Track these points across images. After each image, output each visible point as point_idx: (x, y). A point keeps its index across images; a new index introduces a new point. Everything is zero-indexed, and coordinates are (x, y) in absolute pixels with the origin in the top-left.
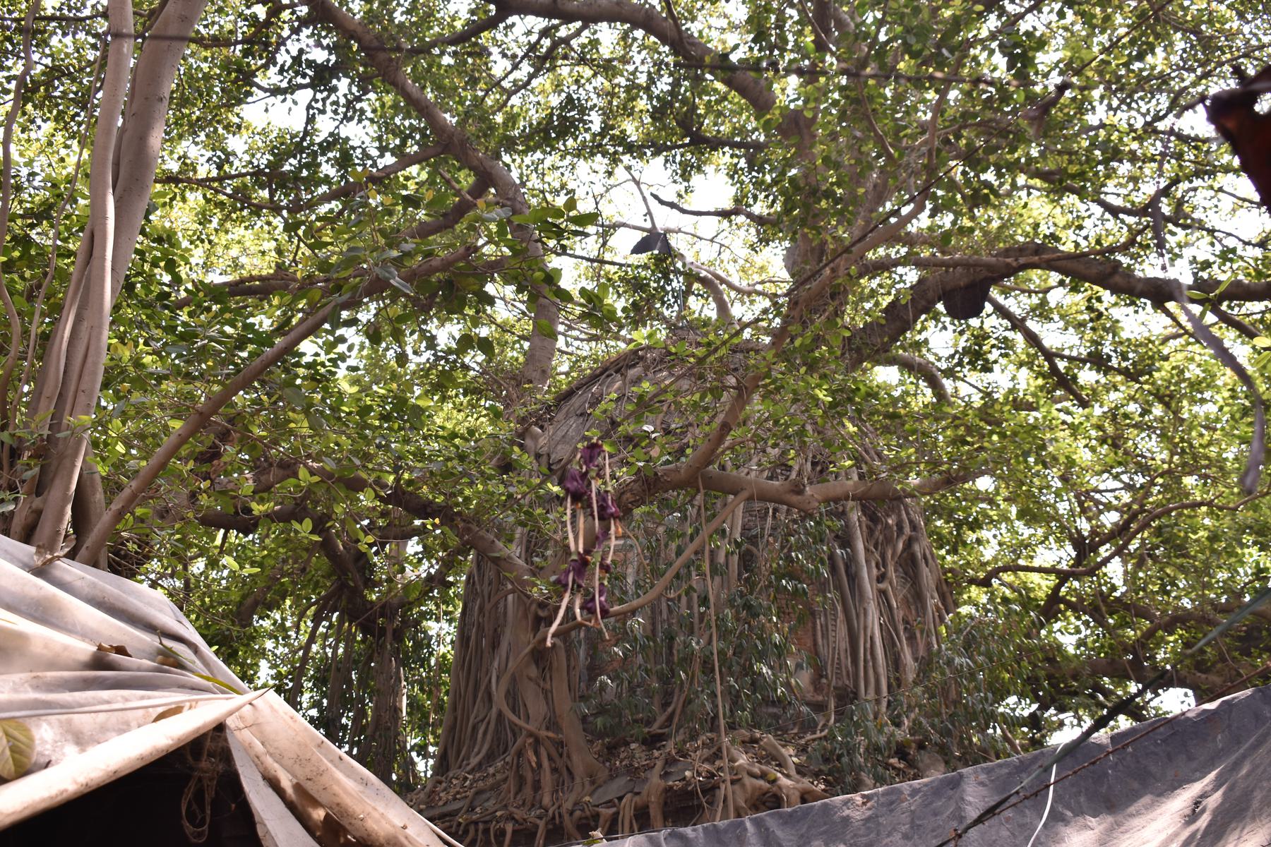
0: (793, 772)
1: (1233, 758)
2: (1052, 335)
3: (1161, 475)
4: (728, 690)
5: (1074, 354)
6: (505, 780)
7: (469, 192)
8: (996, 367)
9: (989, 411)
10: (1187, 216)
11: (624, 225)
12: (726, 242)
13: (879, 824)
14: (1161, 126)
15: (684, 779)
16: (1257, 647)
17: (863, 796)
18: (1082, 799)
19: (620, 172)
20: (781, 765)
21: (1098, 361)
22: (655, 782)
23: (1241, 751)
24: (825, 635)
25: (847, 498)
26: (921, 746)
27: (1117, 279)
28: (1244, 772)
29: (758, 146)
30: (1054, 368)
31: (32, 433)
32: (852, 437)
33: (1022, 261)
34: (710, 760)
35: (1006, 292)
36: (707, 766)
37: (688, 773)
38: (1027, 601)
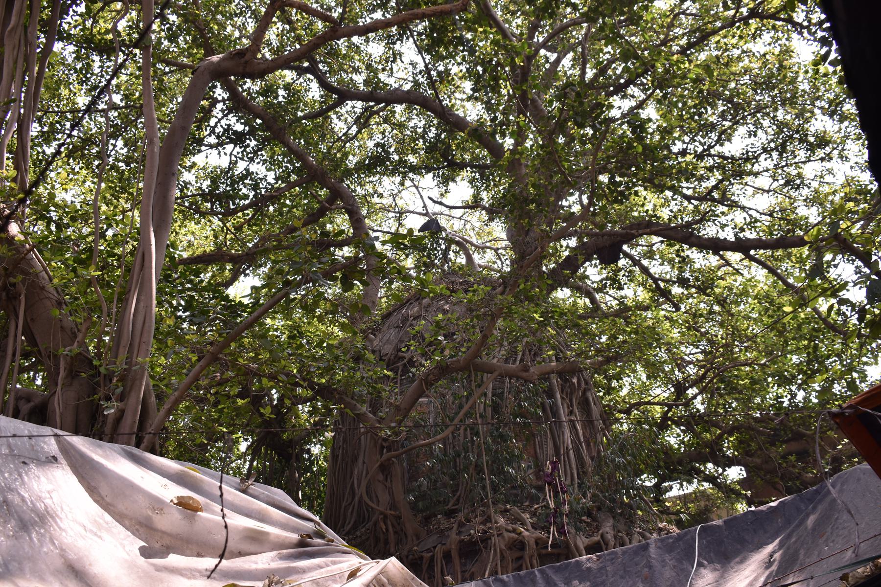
0: (530, 528)
1: (788, 531)
2: (656, 268)
3: (722, 347)
4: (492, 482)
5: (668, 277)
6: (367, 539)
7: (327, 202)
8: (625, 287)
9: (624, 310)
10: (728, 200)
11: (412, 212)
12: (469, 219)
13: (607, 571)
14: (712, 151)
15: (470, 534)
16: (779, 441)
17: (597, 556)
18: (712, 554)
19: (408, 183)
20: (523, 524)
21: (683, 282)
22: (454, 537)
23: (791, 528)
24: (541, 447)
25: (553, 373)
26: (599, 509)
27: (693, 239)
28: (793, 540)
29: (486, 167)
30: (658, 286)
31: (117, 367)
32: (552, 337)
33: (640, 232)
34: (483, 523)
35: (633, 246)
36: (482, 527)
37: (472, 532)
38: (653, 423)
